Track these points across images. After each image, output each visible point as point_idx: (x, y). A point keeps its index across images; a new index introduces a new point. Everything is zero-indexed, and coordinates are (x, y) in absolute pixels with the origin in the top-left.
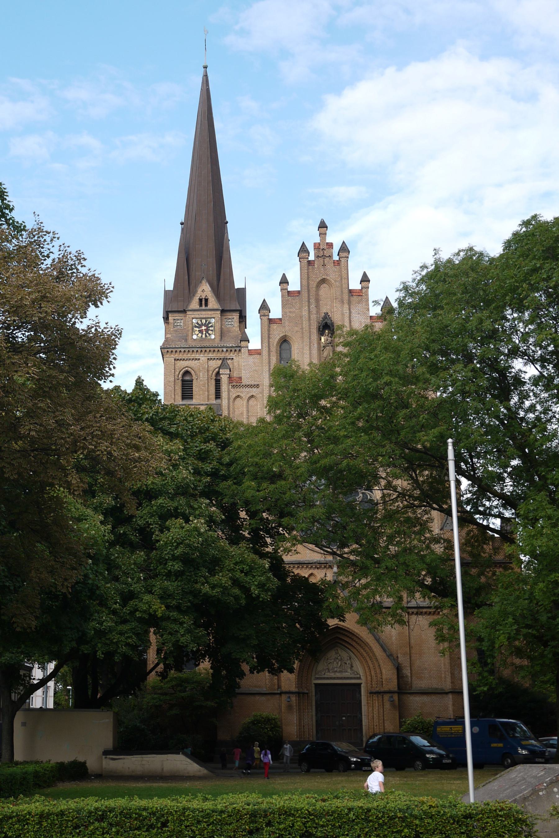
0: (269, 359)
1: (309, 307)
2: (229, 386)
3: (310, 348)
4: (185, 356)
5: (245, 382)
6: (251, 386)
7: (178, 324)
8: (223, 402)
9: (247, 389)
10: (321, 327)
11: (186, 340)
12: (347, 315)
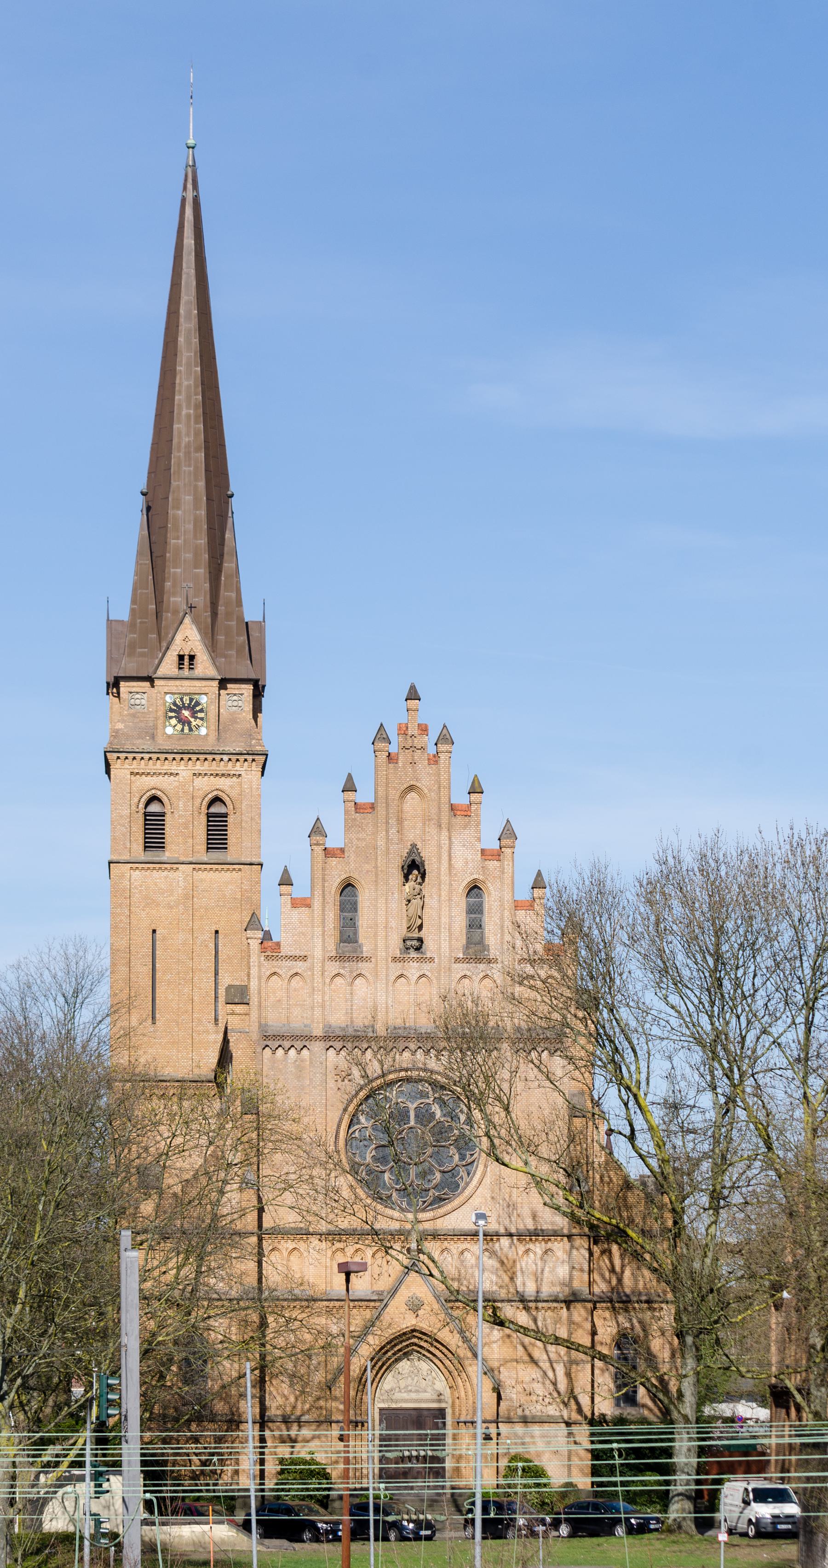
0: (323, 915)
1: (387, 832)
2: (259, 956)
3: (387, 900)
4: (151, 767)
5: (285, 950)
6: (295, 958)
7: (138, 702)
8: (252, 984)
9: (289, 963)
10: (406, 867)
11: (153, 737)
12: (445, 848)
